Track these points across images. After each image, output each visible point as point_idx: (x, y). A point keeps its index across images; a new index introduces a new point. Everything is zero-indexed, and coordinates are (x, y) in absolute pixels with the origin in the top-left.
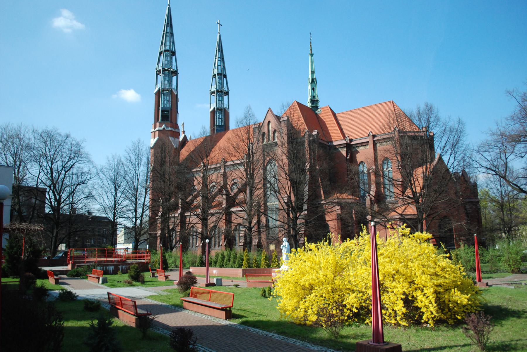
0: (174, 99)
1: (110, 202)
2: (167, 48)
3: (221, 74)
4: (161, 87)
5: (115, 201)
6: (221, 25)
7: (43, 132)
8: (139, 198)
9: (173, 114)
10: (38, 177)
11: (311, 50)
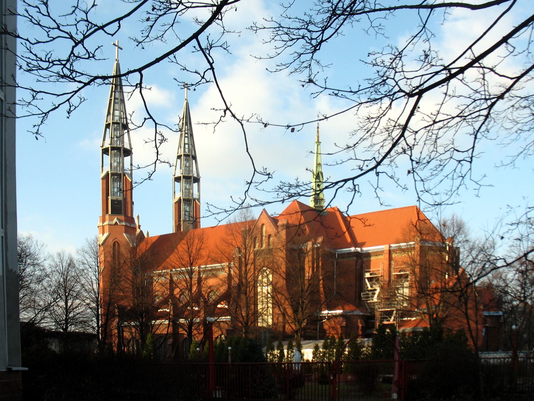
2: (117, 119)
3: (117, 123)
4: (109, 170)
6: (121, 49)
11: (318, 137)
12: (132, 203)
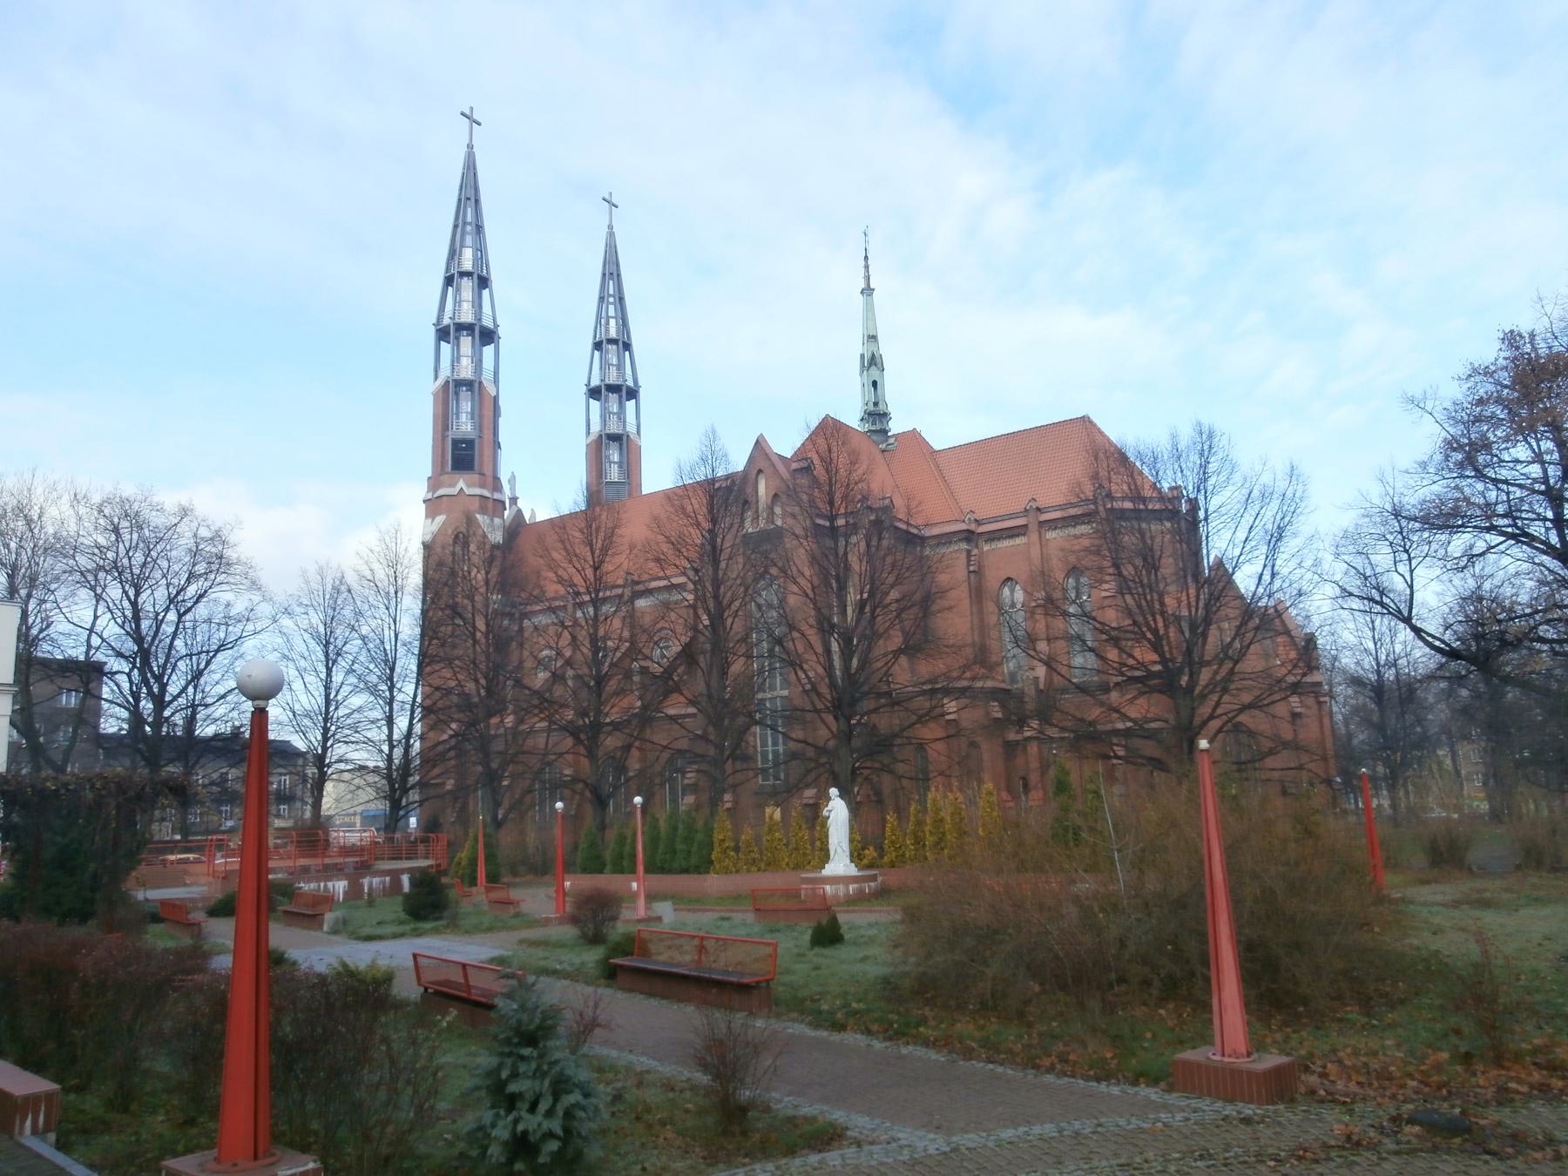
0: (489, 410)
1: (311, 698)
5: (327, 696)
7: (108, 501)
8: (398, 686)
9: (487, 452)
10: (91, 630)
12: (497, 445)
